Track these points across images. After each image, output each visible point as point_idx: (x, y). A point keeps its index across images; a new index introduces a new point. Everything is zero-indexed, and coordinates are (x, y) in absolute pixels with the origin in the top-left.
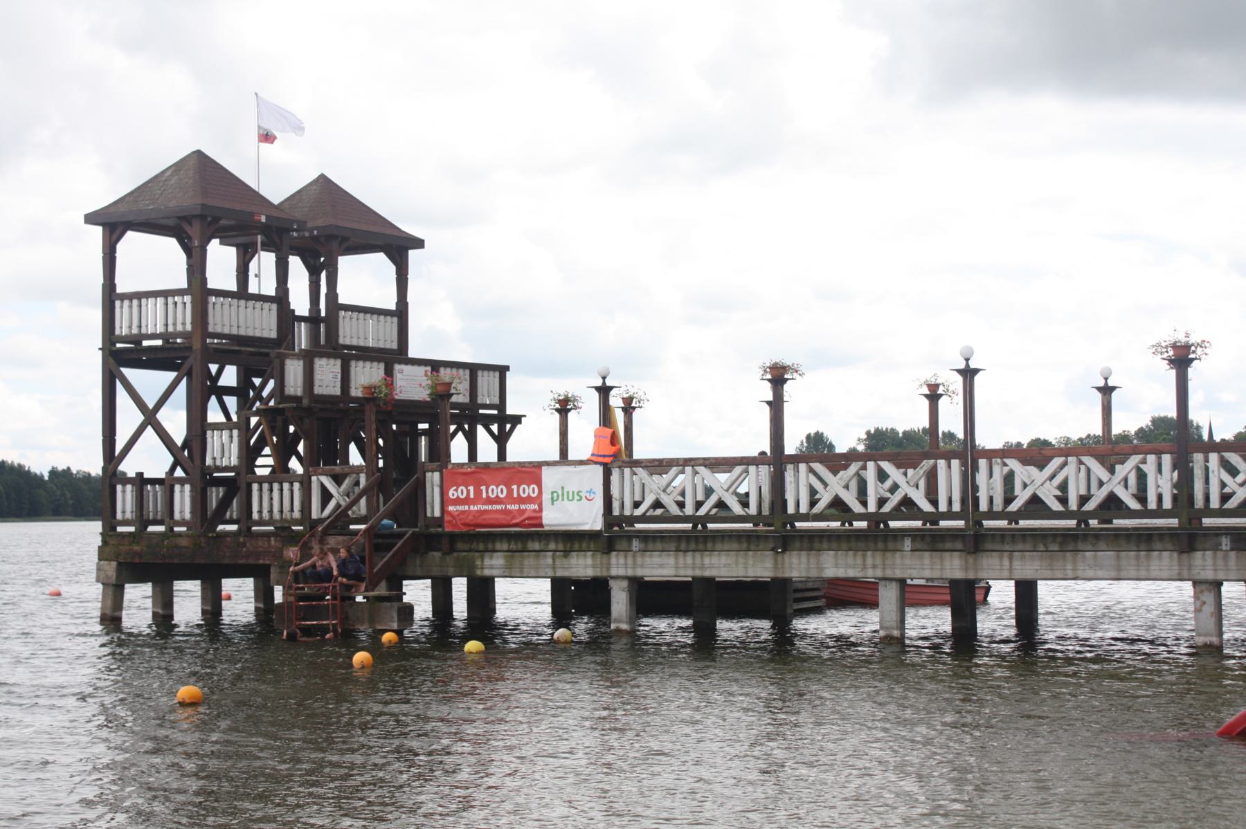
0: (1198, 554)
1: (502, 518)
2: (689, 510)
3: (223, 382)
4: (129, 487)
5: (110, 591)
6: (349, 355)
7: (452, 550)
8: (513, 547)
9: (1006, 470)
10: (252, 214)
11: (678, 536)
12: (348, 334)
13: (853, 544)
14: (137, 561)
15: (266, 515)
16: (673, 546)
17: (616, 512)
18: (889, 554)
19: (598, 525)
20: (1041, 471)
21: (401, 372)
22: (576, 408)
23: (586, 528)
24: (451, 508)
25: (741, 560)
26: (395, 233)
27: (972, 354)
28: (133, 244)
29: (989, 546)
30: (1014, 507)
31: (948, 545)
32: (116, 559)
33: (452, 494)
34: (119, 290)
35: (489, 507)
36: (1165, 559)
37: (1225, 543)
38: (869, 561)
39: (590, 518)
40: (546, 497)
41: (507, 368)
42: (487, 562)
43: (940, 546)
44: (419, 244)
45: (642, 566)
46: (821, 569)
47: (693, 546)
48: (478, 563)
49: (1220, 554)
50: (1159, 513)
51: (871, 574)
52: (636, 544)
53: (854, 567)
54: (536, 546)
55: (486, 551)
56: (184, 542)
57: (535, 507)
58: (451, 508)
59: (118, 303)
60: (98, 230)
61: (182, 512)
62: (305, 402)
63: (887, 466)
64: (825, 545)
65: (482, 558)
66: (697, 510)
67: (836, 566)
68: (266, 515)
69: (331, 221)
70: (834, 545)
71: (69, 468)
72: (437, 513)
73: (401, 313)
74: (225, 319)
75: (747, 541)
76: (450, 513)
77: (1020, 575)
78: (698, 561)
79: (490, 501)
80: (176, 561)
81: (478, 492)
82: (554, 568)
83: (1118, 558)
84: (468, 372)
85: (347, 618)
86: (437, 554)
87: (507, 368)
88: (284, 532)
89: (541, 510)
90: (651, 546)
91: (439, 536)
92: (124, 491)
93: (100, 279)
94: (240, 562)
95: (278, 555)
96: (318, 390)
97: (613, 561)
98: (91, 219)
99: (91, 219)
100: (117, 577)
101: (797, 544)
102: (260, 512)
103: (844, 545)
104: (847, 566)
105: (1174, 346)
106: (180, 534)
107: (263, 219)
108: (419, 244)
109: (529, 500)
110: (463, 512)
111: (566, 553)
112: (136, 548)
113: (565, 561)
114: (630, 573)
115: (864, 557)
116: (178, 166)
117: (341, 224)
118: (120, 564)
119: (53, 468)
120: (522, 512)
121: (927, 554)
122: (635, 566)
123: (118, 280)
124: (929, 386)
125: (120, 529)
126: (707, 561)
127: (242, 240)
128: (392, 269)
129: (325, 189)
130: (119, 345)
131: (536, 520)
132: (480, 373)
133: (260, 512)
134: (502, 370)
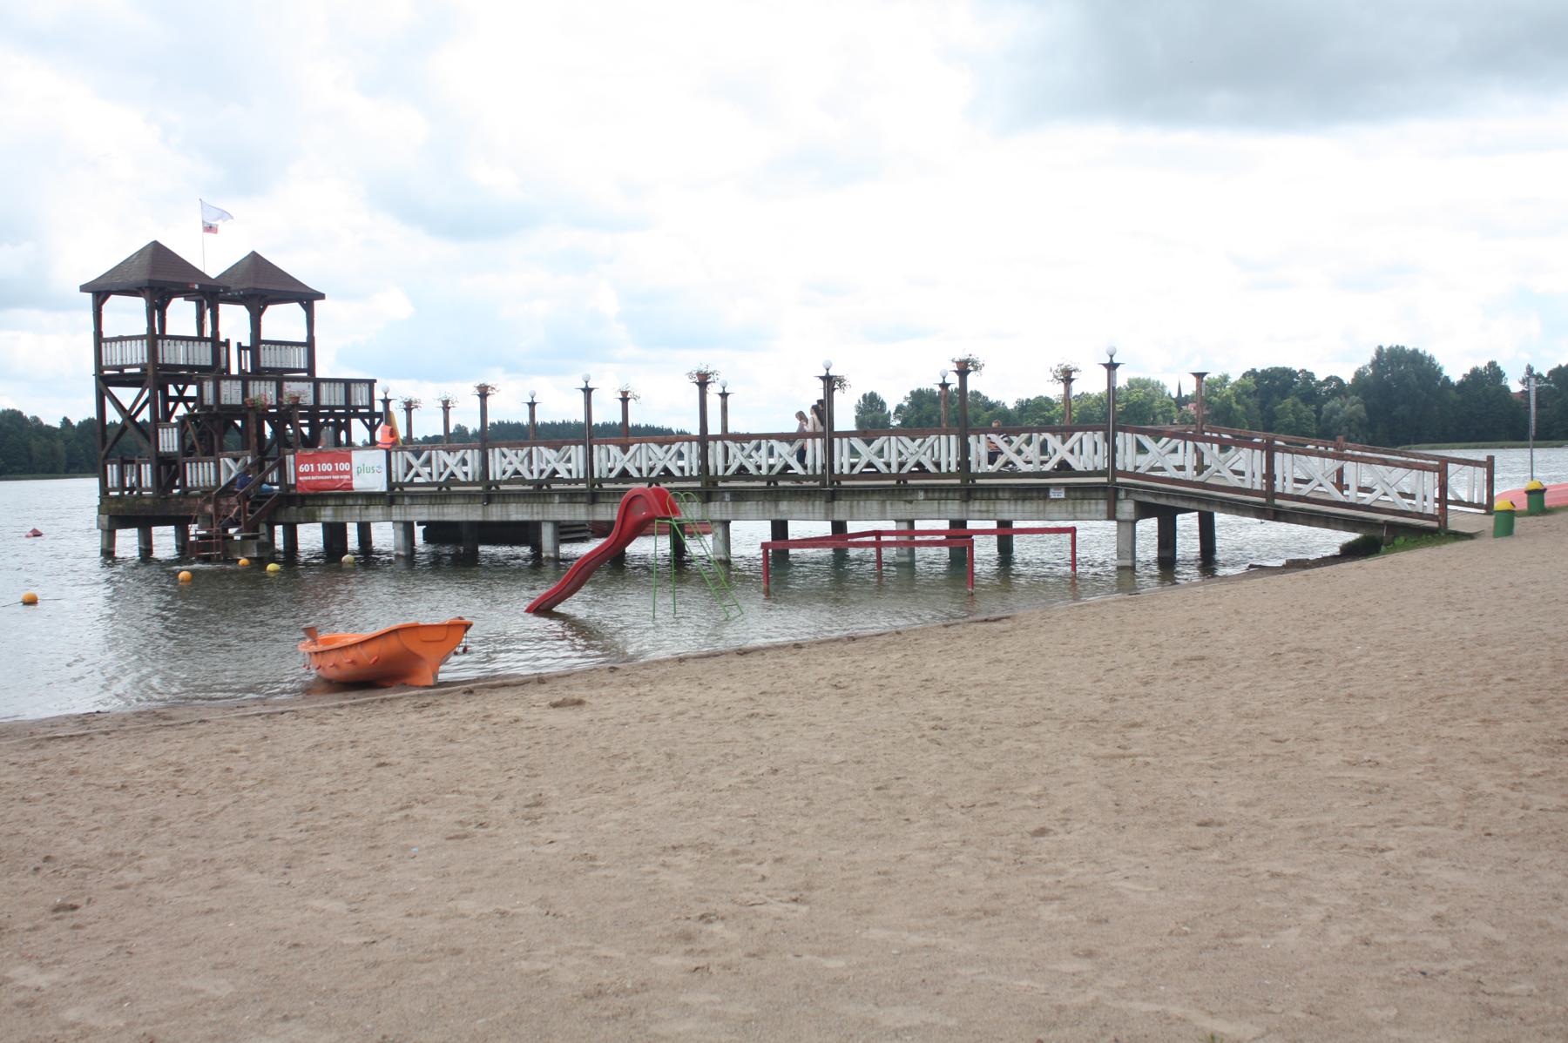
0: (712, 504)
1: (330, 485)
2: (894, 469)
3: (186, 394)
4: (694, 444)
5: (106, 534)
6: (279, 376)
7: (303, 505)
8: (338, 503)
9: (1041, 438)
10: (188, 284)
11: (430, 496)
12: (268, 359)
13: (527, 499)
14: (120, 514)
15: (195, 483)
16: (427, 501)
17: (394, 480)
18: (546, 505)
19: (384, 489)
20: (869, 446)
21: (289, 387)
22: (416, 407)
23: (377, 490)
24: (301, 478)
25: (465, 510)
26: (303, 290)
27: (589, 378)
28: (114, 303)
29: (601, 500)
30: (729, 472)
31: (579, 500)
32: (108, 514)
33: (301, 469)
34: (105, 336)
35: (322, 478)
36: (819, 506)
37: (727, 496)
38: (535, 510)
39: (378, 484)
40: (354, 471)
41: (375, 381)
42: (323, 513)
43: (574, 500)
44: (321, 296)
45: (410, 514)
46: (508, 515)
47: (438, 501)
48: (318, 513)
49: (724, 504)
50: (691, 478)
51: (536, 518)
52: (407, 501)
53: (527, 513)
54: (350, 502)
55: (322, 505)
56: (147, 502)
57: (347, 477)
58: (301, 478)
59: (103, 345)
60: (89, 296)
61: (112, 482)
62: (215, 409)
63: (505, 450)
64: (512, 500)
65: (320, 510)
66: (900, 469)
67: (517, 513)
68: (195, 483)
69: (251, 285)
70: (517, 500)
71: (1495, 372)
72: (293, 482)
73: (310, 345)
74: (175, 355)
75: (469, 497)
76: (300, 482)
77: (837, 517)
78: (1041, 508)
79: (323, 473)
80: (143, 514)
81: (316, 468)
82: (360, 516)
83: (851, 507)
84: (343, 385)
85: (228, 550)
86: (294, 508)
87: (375, 381)
88: (206, 493)
89: (352, 479)
90: (415, 502)
91: (294, 496)
92: (112, 469)
93: (92, 329)
94: (181, 514)
95: (202, 509)
96: (223, 402)
97: (394, 511)
98: (84, 288)
99: (84, 288)
100: (109, 525)
101: (496, 500)
102: (192, 482)
103: (522, 500)
104: (523, 513)
105: (699, 374)
106: (145, 497)
107: (196, 287)
108: (321, 296)
109: (345, 473)
110: (308, 481)
111: (367, 506)
112: (120, 506)
113: (367, 512)
114: (403, 519)
115: (532, 507)
116: (141, 252)
117: (259, 286)
118: (111, 517)
119: (1492, 365)
120: (341, 480)
121: (566, 505)
122: (405, 515)
123: (103, 330)
124: (622, 392)
125: (111, 494)
126: (446, 510)
127: (197, 298)
128: (303, 313)
129: (255, 263)
130: (106, 372)
131: (349, 486)
132: (353, 385)
133: (192, 482)
134: (371, 383)
